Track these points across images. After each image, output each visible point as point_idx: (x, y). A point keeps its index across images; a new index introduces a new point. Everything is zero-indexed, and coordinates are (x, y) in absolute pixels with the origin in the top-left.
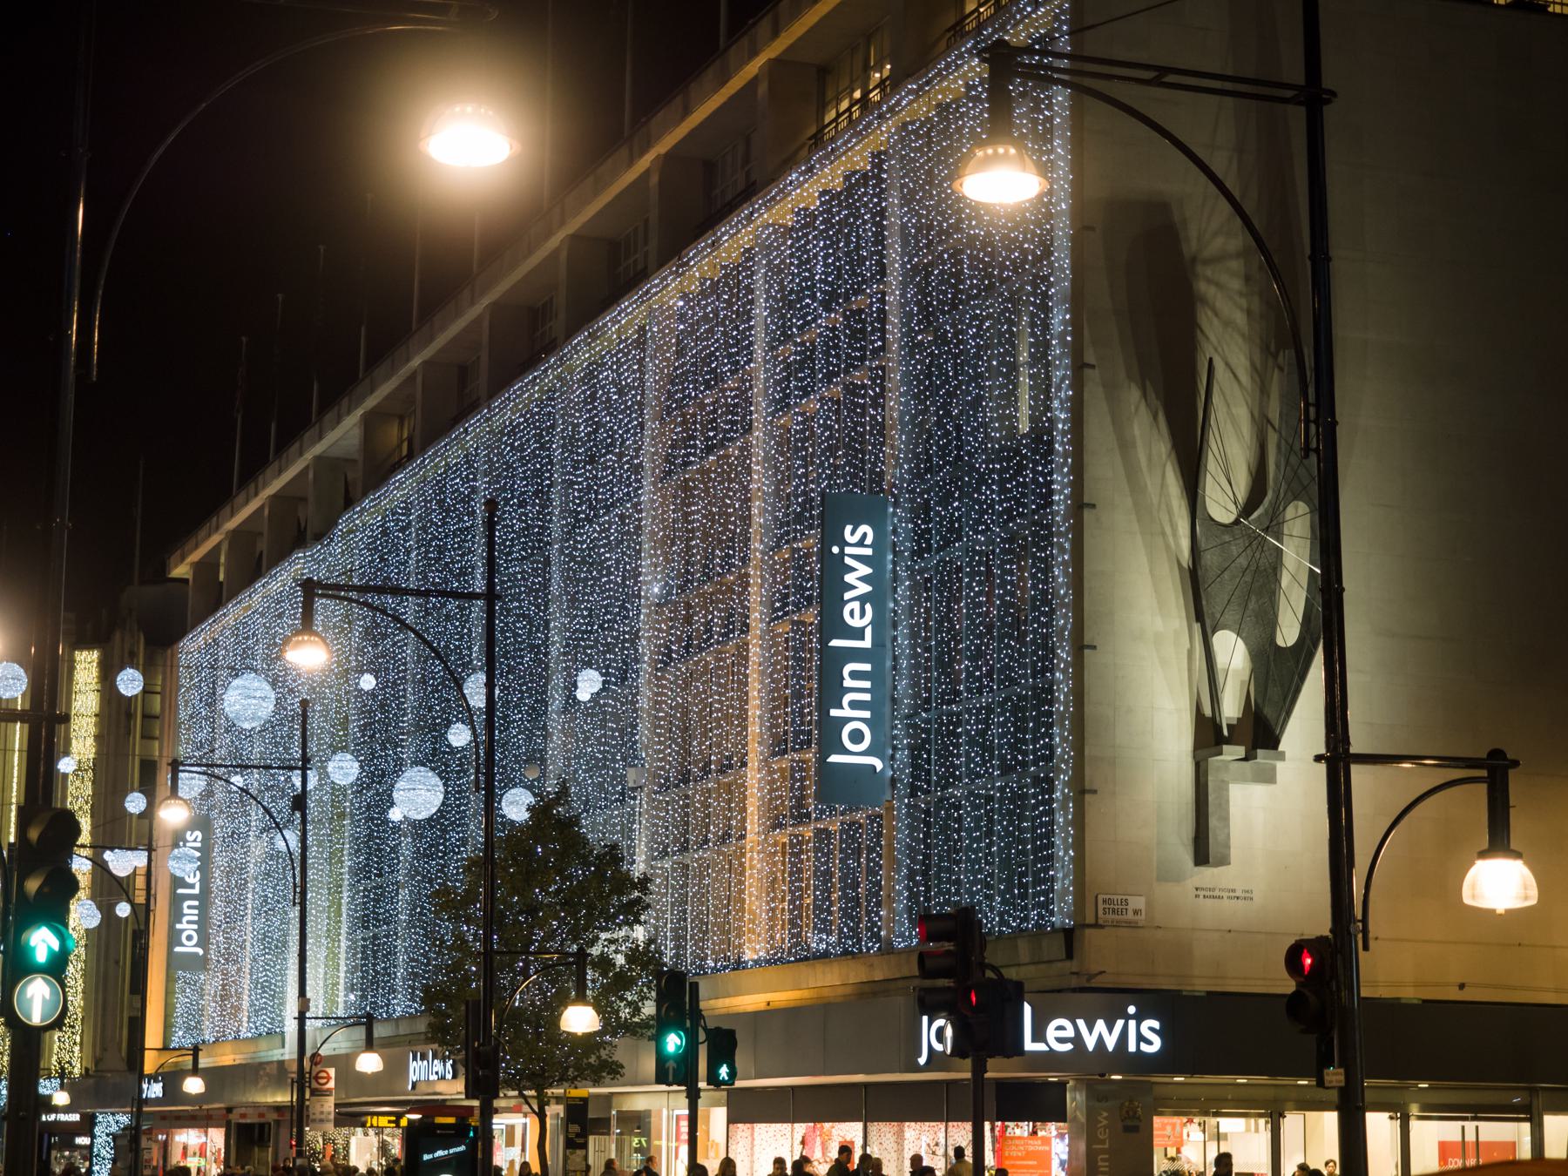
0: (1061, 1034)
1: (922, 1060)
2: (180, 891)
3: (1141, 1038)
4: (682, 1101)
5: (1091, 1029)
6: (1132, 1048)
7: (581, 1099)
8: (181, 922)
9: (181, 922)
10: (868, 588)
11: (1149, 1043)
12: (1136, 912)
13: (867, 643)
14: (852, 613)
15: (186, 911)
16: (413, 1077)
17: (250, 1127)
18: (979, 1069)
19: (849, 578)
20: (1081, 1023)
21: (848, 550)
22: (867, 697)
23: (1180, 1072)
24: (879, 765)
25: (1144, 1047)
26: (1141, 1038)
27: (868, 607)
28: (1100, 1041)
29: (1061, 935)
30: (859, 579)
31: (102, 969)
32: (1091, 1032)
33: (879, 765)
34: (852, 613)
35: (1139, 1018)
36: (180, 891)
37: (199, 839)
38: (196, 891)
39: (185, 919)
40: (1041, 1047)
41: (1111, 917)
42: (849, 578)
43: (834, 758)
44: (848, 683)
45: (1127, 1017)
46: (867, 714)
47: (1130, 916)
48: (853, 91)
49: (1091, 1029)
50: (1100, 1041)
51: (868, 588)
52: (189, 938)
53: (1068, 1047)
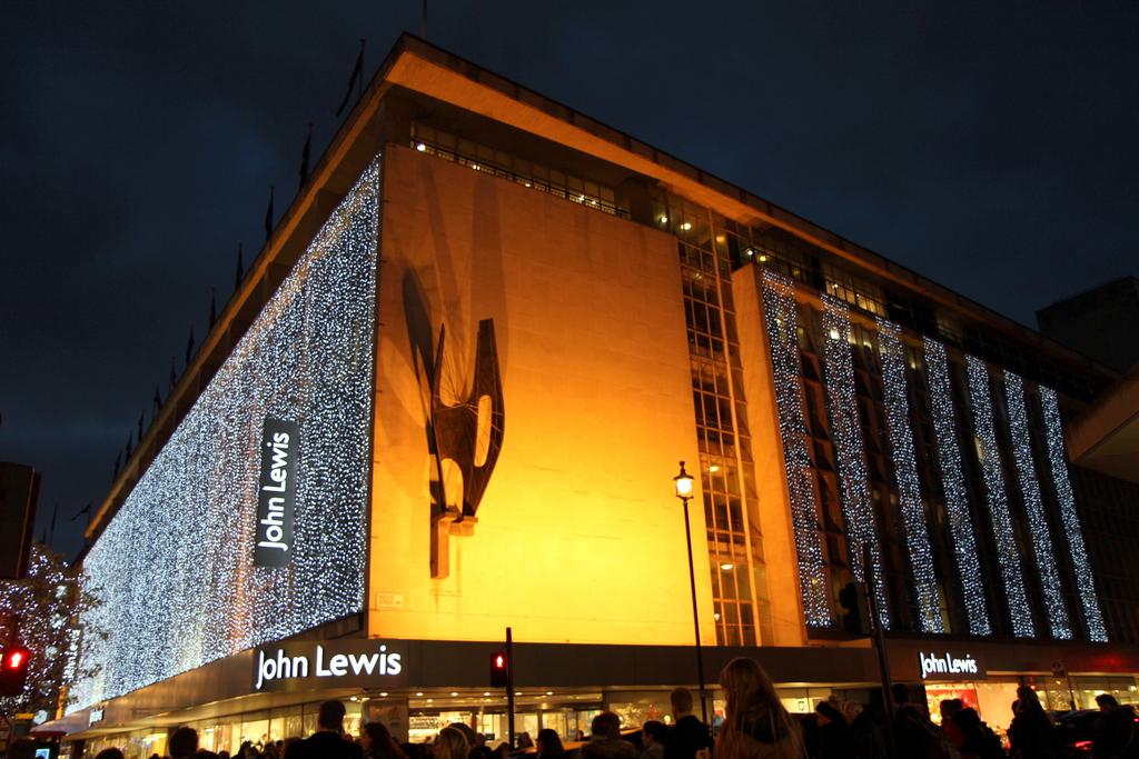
0: (340, 665)
1: (259, 686)
2: (266, 488)
3: (388, 665)
4: (300, 720)
5: (357, 660)
6: (382, 671)
7: (27, 720)
8: (266, 518)
9: (266, 518)
10: (284, 463)
12: (398, 603)
14: (340, 661)
15: (271, 507)
16: (91, 721)
19: (364, 658)
20: (352, 657)
22: (281, 515)
23: (615, 685)
25: (390, 671)
26: (388, 665)
28: (363, 669)
29: (357, 618)
31: (859, 519)
35: (387, 653)
36: (266, 488)
37: (287, 441)
38: (282, 489)
39: (270, 515)
40: (327, 673)
41: (384, 605)
42: (364, 658)
45: (380, 653)
46: (281, 523)
47: (395, 605)
48: (764, 254)
49: (357, 660)
50: (363, 669)
51: (284, 463)
52: (274, 534)
53: (344, 672)
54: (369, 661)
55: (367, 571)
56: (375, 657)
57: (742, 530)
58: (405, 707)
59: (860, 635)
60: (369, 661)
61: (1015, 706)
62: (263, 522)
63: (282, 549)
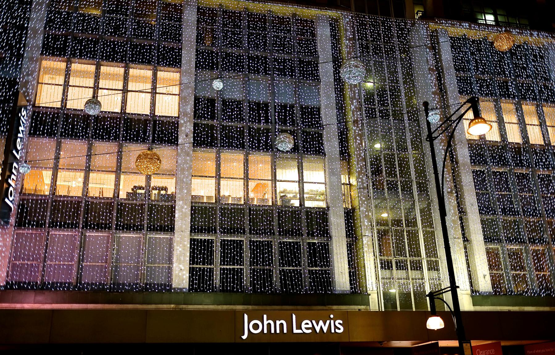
3: (336, 327)
6: (333, 331)
10: (318, 331)
11: (339, 329)
13: (295, 331)
14: (307, 324)
17: (258, 104)
18: (427, 296)
20: (314, 322)
21: (332, 322)
22: (273, 331)
24: (244, 337)
25: (337, 331)
26: (336, 327)
27: (310, 331)
30: (321, 327)
32: (318, 325)
33: (244, 337)
34: (307, 324)
40: (300, 331)
43: (246, 317)
44: (278, 323)
45: (331, 319)
51: (318, 331)
52: (256, 327)
53: (310, 331)
54: (325, 325)
55: (365, 276)
56: (328, 322)
57: (419, 255)
58: (469, 344)
59: (503, 347)
60: (325, 325)
61: (139, 186)
62: (265, 316)
63: (243, 335)
